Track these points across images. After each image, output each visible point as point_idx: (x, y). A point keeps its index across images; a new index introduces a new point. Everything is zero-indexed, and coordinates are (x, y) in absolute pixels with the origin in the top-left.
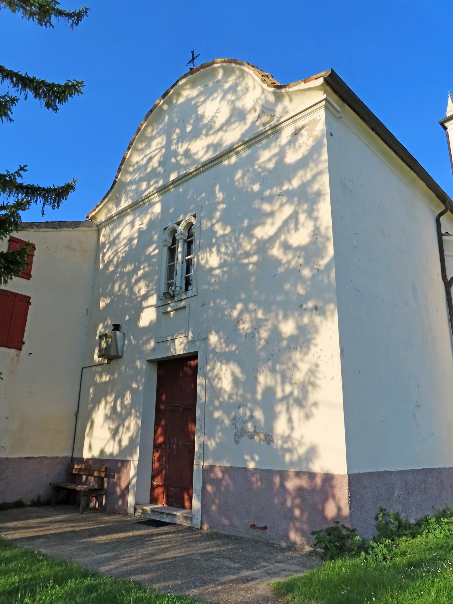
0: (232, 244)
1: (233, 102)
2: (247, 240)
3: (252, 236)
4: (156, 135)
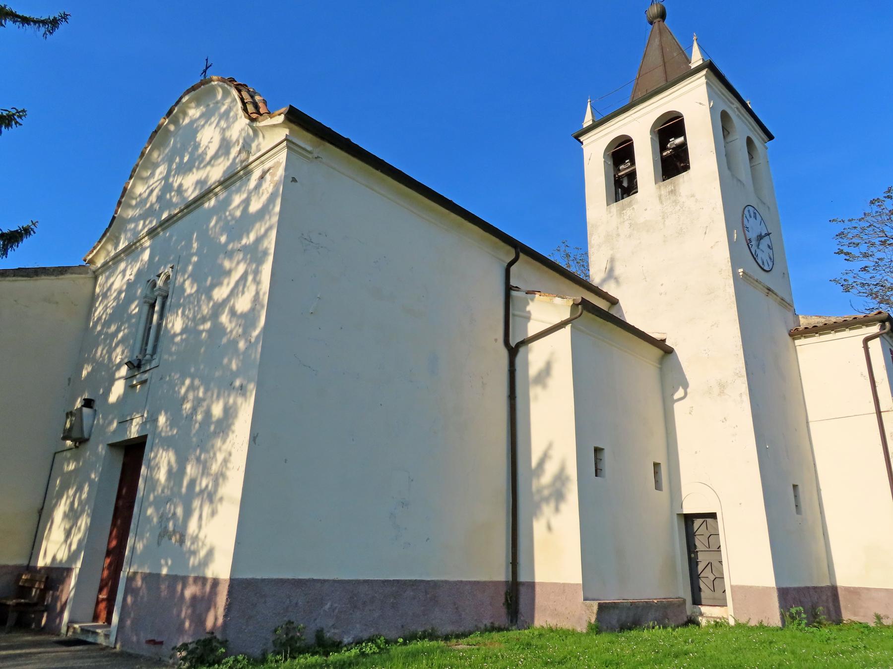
3: (210, 298)
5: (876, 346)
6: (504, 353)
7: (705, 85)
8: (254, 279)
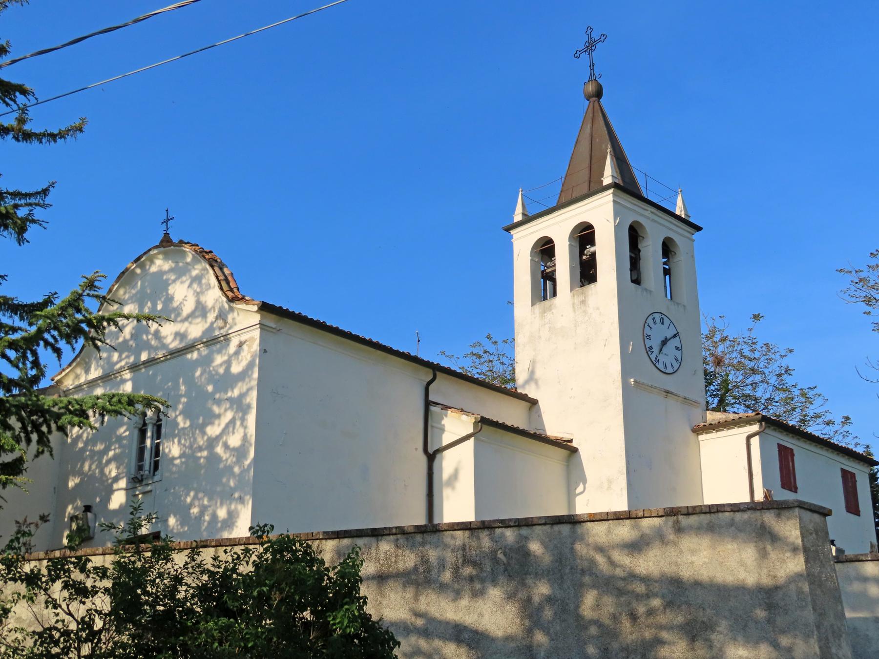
0: (190, 438)
1: (198, 294)
2: (200, 435)
3: (204, 433)
4: (128, 299)
5: (755, 442)
6: (423, 460)
7: (612, 203)
8: (242, 424)
